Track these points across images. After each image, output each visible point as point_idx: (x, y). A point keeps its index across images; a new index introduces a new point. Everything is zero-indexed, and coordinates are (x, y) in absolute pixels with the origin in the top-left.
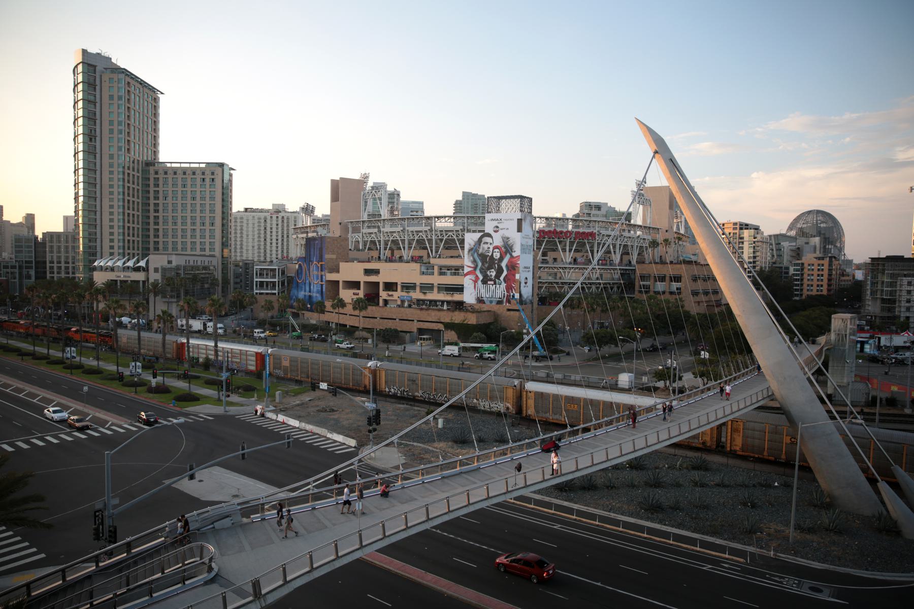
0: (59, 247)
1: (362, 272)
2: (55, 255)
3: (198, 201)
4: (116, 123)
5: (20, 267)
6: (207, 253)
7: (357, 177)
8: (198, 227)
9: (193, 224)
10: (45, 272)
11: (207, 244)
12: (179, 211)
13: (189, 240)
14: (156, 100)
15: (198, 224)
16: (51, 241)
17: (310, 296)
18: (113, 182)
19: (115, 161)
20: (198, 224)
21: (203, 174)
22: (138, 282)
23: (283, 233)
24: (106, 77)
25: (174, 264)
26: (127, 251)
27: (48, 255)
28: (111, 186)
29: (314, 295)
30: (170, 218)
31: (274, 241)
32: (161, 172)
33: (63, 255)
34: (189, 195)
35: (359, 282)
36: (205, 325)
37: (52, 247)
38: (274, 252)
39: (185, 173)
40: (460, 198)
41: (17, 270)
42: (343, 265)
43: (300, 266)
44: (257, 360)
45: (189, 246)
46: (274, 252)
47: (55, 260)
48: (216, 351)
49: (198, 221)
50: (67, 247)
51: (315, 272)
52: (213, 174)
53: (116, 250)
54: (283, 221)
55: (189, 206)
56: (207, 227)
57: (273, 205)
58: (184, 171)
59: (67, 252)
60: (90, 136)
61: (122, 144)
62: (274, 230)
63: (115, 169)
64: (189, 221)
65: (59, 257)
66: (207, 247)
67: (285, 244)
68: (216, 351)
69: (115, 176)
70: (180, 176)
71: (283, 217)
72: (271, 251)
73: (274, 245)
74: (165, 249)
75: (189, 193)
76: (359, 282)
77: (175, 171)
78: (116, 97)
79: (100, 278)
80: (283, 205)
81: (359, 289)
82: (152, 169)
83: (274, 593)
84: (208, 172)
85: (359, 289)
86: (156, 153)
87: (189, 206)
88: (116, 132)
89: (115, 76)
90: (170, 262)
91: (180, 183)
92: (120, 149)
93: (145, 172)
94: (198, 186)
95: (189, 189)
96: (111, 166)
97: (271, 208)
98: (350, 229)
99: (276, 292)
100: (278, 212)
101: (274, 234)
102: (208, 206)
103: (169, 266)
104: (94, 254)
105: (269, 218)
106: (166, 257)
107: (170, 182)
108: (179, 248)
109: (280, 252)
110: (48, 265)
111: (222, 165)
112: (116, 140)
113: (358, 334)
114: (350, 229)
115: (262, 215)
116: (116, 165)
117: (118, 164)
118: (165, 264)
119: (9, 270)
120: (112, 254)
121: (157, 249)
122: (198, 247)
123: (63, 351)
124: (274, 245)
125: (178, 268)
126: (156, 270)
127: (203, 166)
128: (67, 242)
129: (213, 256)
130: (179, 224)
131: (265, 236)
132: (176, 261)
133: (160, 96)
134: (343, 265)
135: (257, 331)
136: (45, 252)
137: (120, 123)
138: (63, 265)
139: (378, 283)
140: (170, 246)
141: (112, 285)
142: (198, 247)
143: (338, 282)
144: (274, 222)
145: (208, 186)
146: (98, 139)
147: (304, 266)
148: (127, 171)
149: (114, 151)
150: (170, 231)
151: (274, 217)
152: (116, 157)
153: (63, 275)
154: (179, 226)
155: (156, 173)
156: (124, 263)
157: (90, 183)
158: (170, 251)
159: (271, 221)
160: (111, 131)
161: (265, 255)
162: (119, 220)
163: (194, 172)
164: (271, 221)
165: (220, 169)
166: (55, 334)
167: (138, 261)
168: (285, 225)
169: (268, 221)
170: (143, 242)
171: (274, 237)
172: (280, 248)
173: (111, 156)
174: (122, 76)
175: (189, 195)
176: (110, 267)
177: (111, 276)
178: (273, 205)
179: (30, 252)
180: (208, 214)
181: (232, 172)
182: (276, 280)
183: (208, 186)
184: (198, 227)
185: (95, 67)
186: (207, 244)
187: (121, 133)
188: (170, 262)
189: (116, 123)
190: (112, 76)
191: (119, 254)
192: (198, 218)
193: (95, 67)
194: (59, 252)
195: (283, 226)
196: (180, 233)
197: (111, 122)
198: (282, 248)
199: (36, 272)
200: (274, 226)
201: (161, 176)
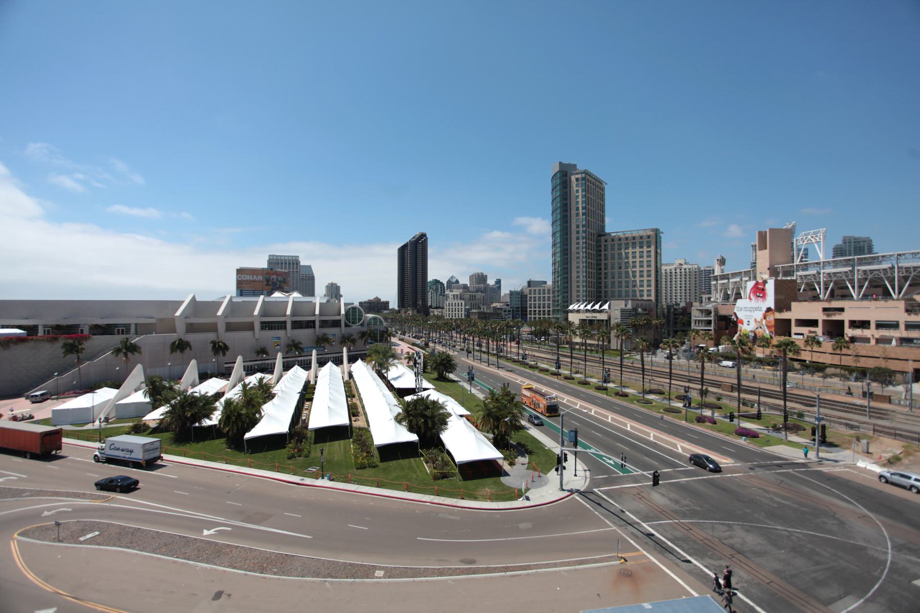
8: (645, 278)
30: (631, 273)
32: (609, 240)
82: (603, 238)
83: (441, 502)
86: (603, 227)
99: (712, 328)
113: (829, 371)
130: (616, 277)
139: (790, 320)
141: (583, 321)
143: (790, 320)
155: (606, 241)
177: (583, 316)
201: (609, 243)
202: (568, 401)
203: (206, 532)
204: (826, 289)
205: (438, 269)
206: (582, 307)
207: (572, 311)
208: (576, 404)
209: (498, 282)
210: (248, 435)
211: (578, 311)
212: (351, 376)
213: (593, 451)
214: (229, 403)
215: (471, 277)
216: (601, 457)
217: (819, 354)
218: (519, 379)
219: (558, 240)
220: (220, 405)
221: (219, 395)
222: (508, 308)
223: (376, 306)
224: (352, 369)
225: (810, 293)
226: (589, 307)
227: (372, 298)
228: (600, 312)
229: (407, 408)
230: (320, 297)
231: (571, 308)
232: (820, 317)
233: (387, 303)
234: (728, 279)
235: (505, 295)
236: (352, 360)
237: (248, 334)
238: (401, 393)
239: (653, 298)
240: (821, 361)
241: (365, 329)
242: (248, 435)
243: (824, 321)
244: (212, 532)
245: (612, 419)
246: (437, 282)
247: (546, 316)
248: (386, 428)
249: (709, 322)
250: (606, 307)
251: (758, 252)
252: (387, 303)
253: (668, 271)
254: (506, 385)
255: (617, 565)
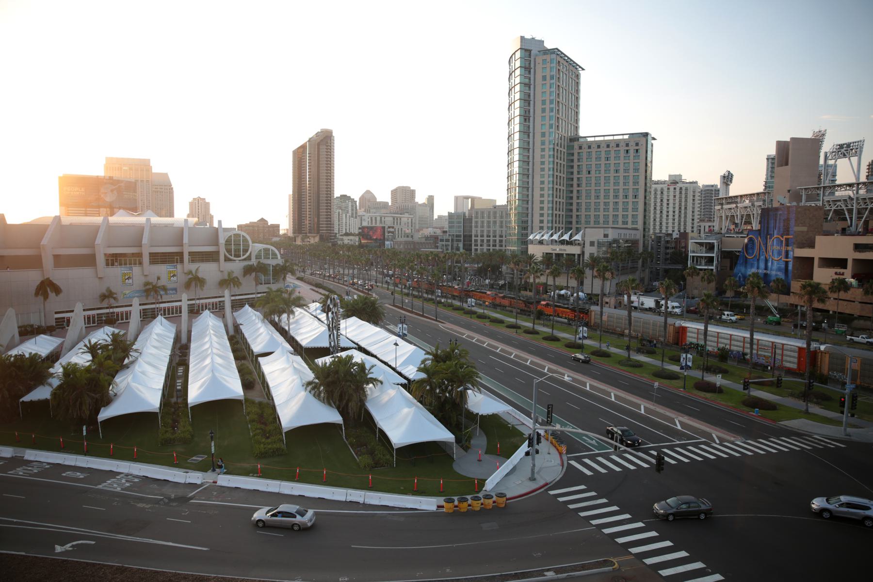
0: (483, 222)
1: (852, 247)
2: (479, 229)
3: (621, 173)
4: (548, 102)
5: (452, 240)
6: (630, 226)
7: (809, 135)
8: (621, 200)
9: (616, 197)
10: (471, 245)
11: (630, 217)
12: (602, 184)
13: (601, 213)
14: (578, 76)
15: (621, 197)
16: (477, 217)
17: (766, 275)
18: (544, 158)
19: (547, 139)
20: (621, 197)
21: (627, 145)
22: (574, 255)
23: (680, 204)
24: (539, 60)
25: (610, 238)
26: (555, 225)
27: (474, 229)
28: (543, 163)
29: (774, 273)
31: (671, 213)
32: (585, 146)
33: (485, 229)
34: (612, 168)
35: (846, 260)
36: (657, 302)
37: (476, 222)
38: (670, 225)
39: (608, 146)
40: (356, 197)
41: (450, 243)
42: (819, 239)
43: (751, 240)
44: (799, 358)
45: (611, 219)
46: (670, 225)
47: (491, 234)
48: (752, 343)
49: (621, 194)
50: (489, 222)
51: (776, 248)
52: (637, 144)
53: (545, 225)
54: (681, 193)
55: (612, 178)
56: (631, 199)
57: (670, 176)
58: (608, 144)
59: (489, 227)
60: (526, 117)
61: (553, 122)
62: (671, 202)
63: (546, 146)
64: (611, 194)
65: (482, 231)
66: (630, 220)
67: (683, 216)
68: (752, 343)
69: (547, 153)
70: (604, 149)
71: (681, 188)
72: (667, 223)
73: (671, 217)
74: (597, 222)
75: (612, 165)
76: (846, 260)
77: (599, 145)
78: (548, 78)
79: (536, 251)
80: (680, 176)
81: (845, 268)
82: (576, 144)
84: (632, 143)
85: (845, 268)
87: (612, 178)
88: (547, 110)
89: (548, 57)
90: (606, 236)
91: (603, 155)
92: (551, 126)
93: (570, 148)
94: (622, 158)
95: (612, 161)
96: (543, 143)
97: (667, 179)
98: (804, 197)
100: (675, 183)
101: (671, 205)
102: (631, 178)
103: (605, 240)
104: (526, 228)
105: (666, 189)
106: (602, 230)
107: (594, 155)
108: (601, 221)
109: (676, 224)
110: (473, 238)
111: (646, 135)
112: (547, 118)
114: (804, 197)
115: (659, 187)
116: (547, 143)
117: (550, 142)
118: (601, 238)
119: (444, 243)
120: (541, 228)
121: (588, 222)
122: (620, 219)
123: (576, 332)
124: (671, 217)
125: (615, 241)
126: (592, 244)
127: (626, 137)
128: (489, 217)
129: (636, 229)
131: (661, 209)
132: (612, 235)
133: (581, 72)
134: (819, 239)
135: (726, 313)
136: (471, 227)
137: (551, 102)
138: (485, 238)
139: (813, 258)
140: (592, 219)
141: (548, 257)
142: (620, 219)
143: (813, 258)
144: (672, 194)
145: (632, 157)
146: (531, 119)
147: (758, 241)
148: (556, 148)
149: (546, 129)
150: (593, 205)
151: (672, 188)
152: (547, 135)
153: (498, 248)
154: (602, 200)
155: (580, 148)
156: (559, 237)
157: (525, 161)
158: (592, 224)
159: (668, 192)
160: (544, 110)
161: (661, 228)
162: (549, 195)
163: (617, 144)
164: (668, 192)
165: (644, 139)
166: (522, 306)
167: (552, 235)
168: (683, 196)
169: (665, 193)
170: (568, 219)
171: (671, 209)
172: (677, 220)
173: (543, 135)
174: (554, 56)
175: (612, 168)
176: (542, 243)
177: (548, 249)
178: (670, 176)
179: (460, 227)
180: (593, 187)
181: (653, 142)
182: (714, 255)
183: (632, 157)
184: (621, 200)
185: (530, 51)
186: (630, 217)
187: (552, 111)
188: (606, 236)
189: (548, 102)
190: (545, 57)
191: (548, 228)
192: (621, 191)
193: (530, 51)
194: (482, 227)
195: (680, 197)
196: (602, 207)
197: (544, 102)
198: (680, 220)
199: (464, 245)
200: (671, 198)
202: (502, 350)
203: (59, 549)
204: (859, 218)
205: (348, 182)
206: (546, 237)
207: (532, 242)
208: (527, 360)
209: (431, 199)
210: (27, 398)
211: (541, 242)
212: (237, 328)
213: (570, 430)
214: (70, 371)
215: (394, 193)
216: (580, 435)
217: (845, 303)
218: (466, 334)
219: (517, 144)
220: (58, 369)
221: (54, 357)
222: (446, 237)
223: (262, 230)
224: (239, 321)
225: (840, 225)
226: (555, 237)
227: (255, 219)
228: (569, 243)
229: (322, 373)
230: (181, 213)
231: (531, 237)
232: (851, 255)
233: (278, 226)
234: (736, 203)
235: (440, 217)
236: (237, 305)
237: (86, 272)
238: (310, 354)
239: (640, 225)
240: (847, 312)
241: (254, 262)
242: (27, 398)
243: (856, 261)
244: (68, 547)
245: (591, 387)
246: (344, 198)
247: (491, 248)
248: (293, 398)
249: (710, 260)
250: (578, 237)
251: (777, 169)
252: (278, 226)
253: (659, 189)
254: (456, 341)
255: (609, 572)
